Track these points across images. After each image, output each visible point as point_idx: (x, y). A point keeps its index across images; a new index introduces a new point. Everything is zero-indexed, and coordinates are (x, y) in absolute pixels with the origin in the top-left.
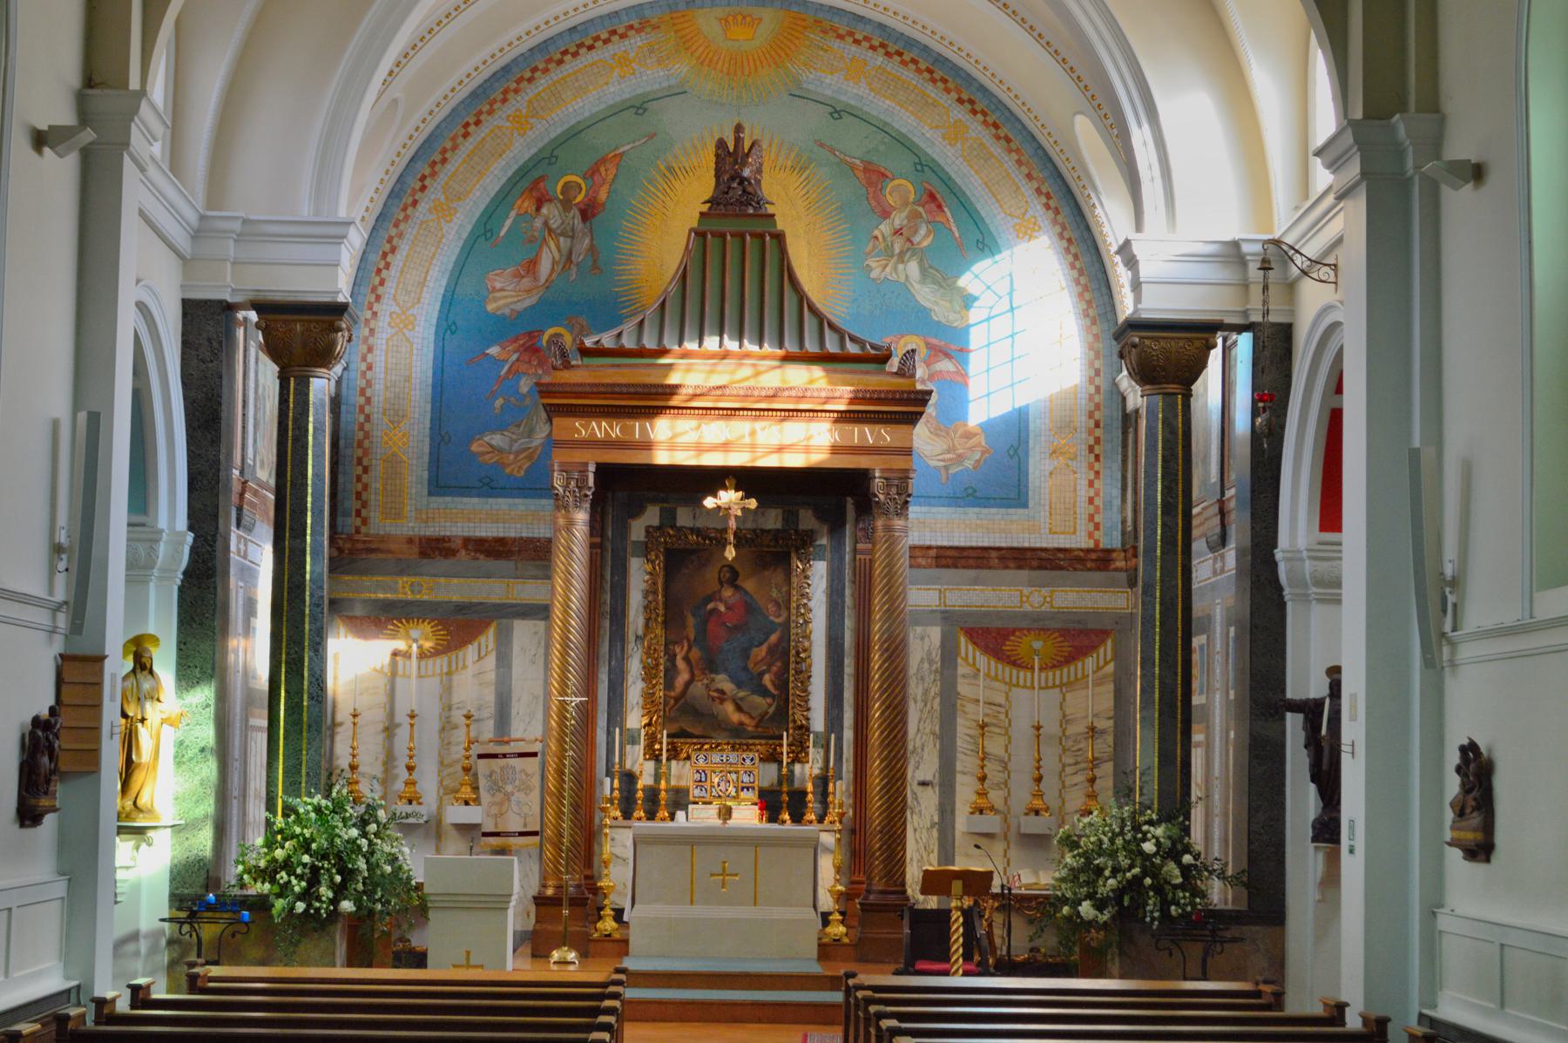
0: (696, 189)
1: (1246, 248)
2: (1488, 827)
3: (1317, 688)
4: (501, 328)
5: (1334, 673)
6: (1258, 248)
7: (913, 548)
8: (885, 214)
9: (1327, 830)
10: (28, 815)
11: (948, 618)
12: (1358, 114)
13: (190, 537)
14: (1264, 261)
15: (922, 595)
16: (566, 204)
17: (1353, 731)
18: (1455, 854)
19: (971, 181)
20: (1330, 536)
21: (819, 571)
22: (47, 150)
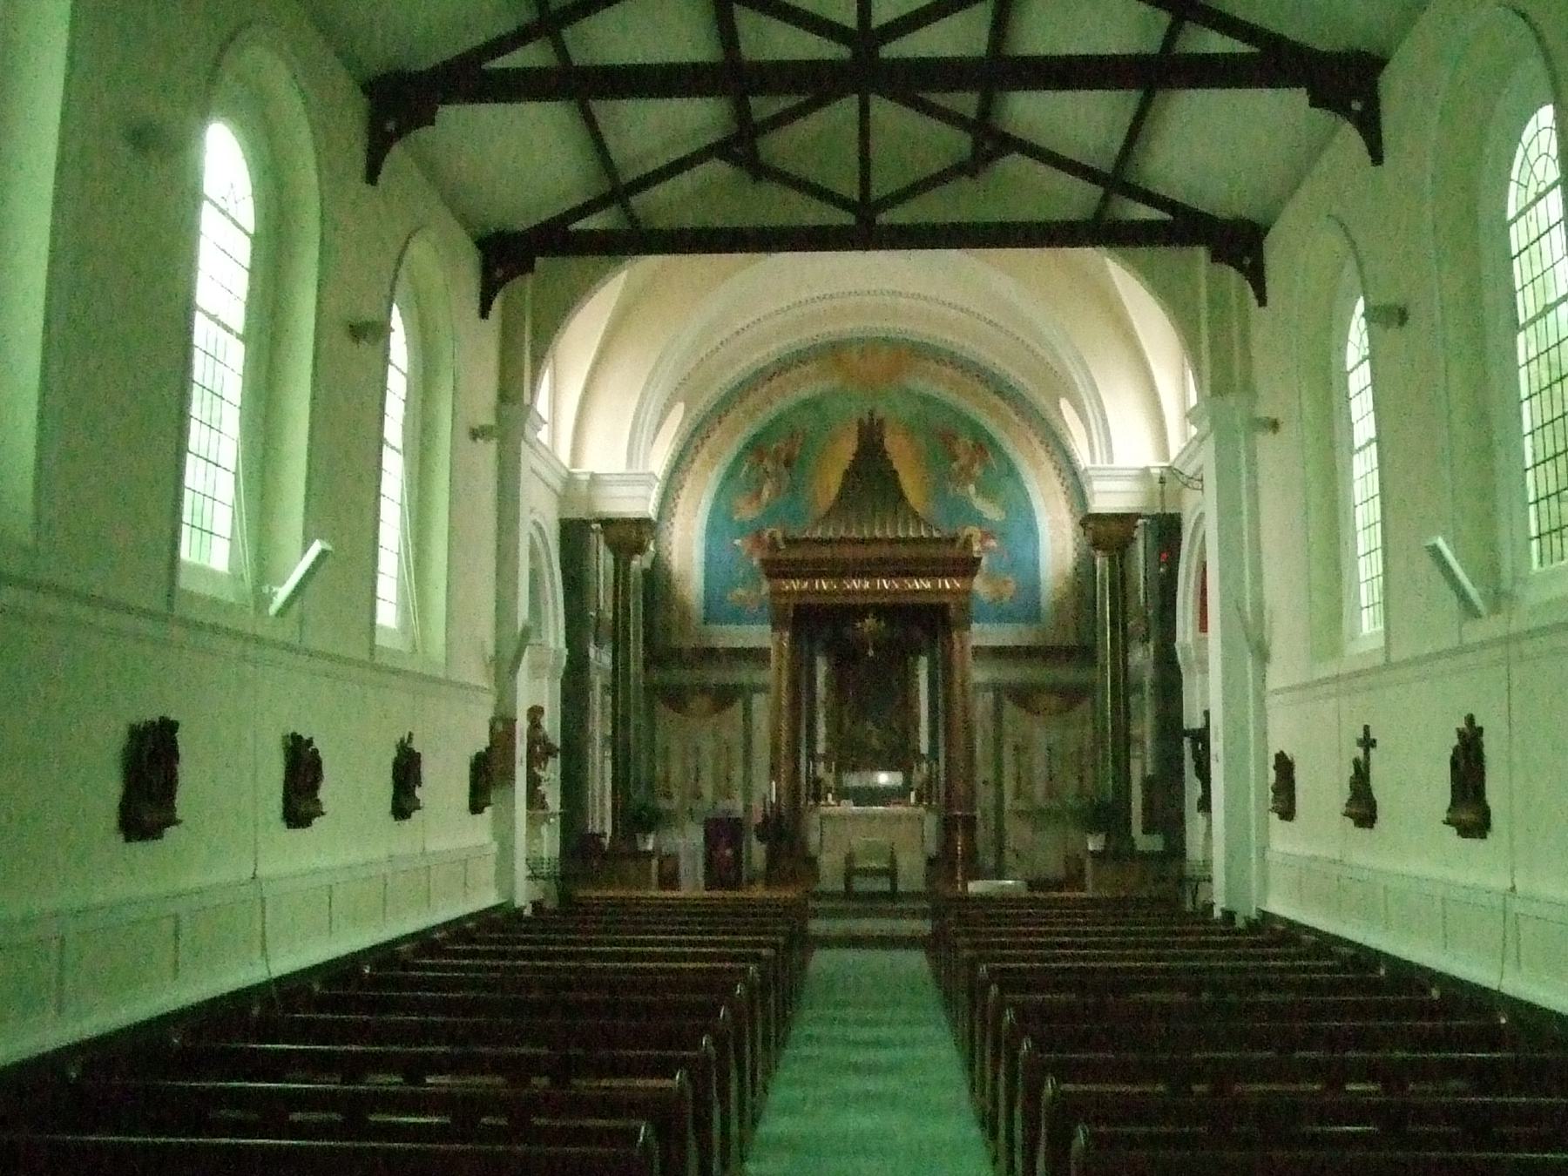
0: (847, 449)
1: (1153, 471)
2: (1291, 798)
3: (1198, 724)
4: (742, 529)
5: (1207, 714)
6: (1157, 471)
7: (973, 647)
8: (955, 458)
9: (1205, 804)
10: (476, 808)
11: (997, 688)
12: (1208, 392)
13: (566, 652)
14: (1161, 478)
15: (980, 674)
16: (776, 460)
17: (1216, 746)
18: (1274, 817)
19: (991, 425)
20: (1203, 634)
21: (924, 661)
22: (478, 440)
